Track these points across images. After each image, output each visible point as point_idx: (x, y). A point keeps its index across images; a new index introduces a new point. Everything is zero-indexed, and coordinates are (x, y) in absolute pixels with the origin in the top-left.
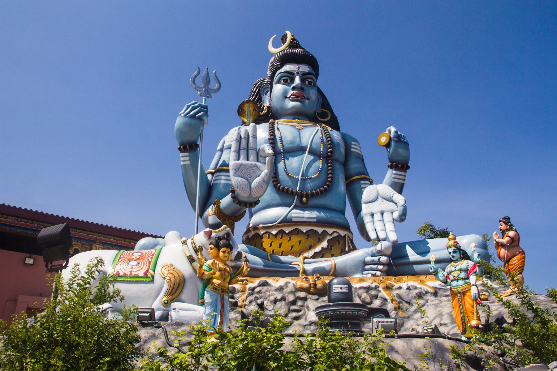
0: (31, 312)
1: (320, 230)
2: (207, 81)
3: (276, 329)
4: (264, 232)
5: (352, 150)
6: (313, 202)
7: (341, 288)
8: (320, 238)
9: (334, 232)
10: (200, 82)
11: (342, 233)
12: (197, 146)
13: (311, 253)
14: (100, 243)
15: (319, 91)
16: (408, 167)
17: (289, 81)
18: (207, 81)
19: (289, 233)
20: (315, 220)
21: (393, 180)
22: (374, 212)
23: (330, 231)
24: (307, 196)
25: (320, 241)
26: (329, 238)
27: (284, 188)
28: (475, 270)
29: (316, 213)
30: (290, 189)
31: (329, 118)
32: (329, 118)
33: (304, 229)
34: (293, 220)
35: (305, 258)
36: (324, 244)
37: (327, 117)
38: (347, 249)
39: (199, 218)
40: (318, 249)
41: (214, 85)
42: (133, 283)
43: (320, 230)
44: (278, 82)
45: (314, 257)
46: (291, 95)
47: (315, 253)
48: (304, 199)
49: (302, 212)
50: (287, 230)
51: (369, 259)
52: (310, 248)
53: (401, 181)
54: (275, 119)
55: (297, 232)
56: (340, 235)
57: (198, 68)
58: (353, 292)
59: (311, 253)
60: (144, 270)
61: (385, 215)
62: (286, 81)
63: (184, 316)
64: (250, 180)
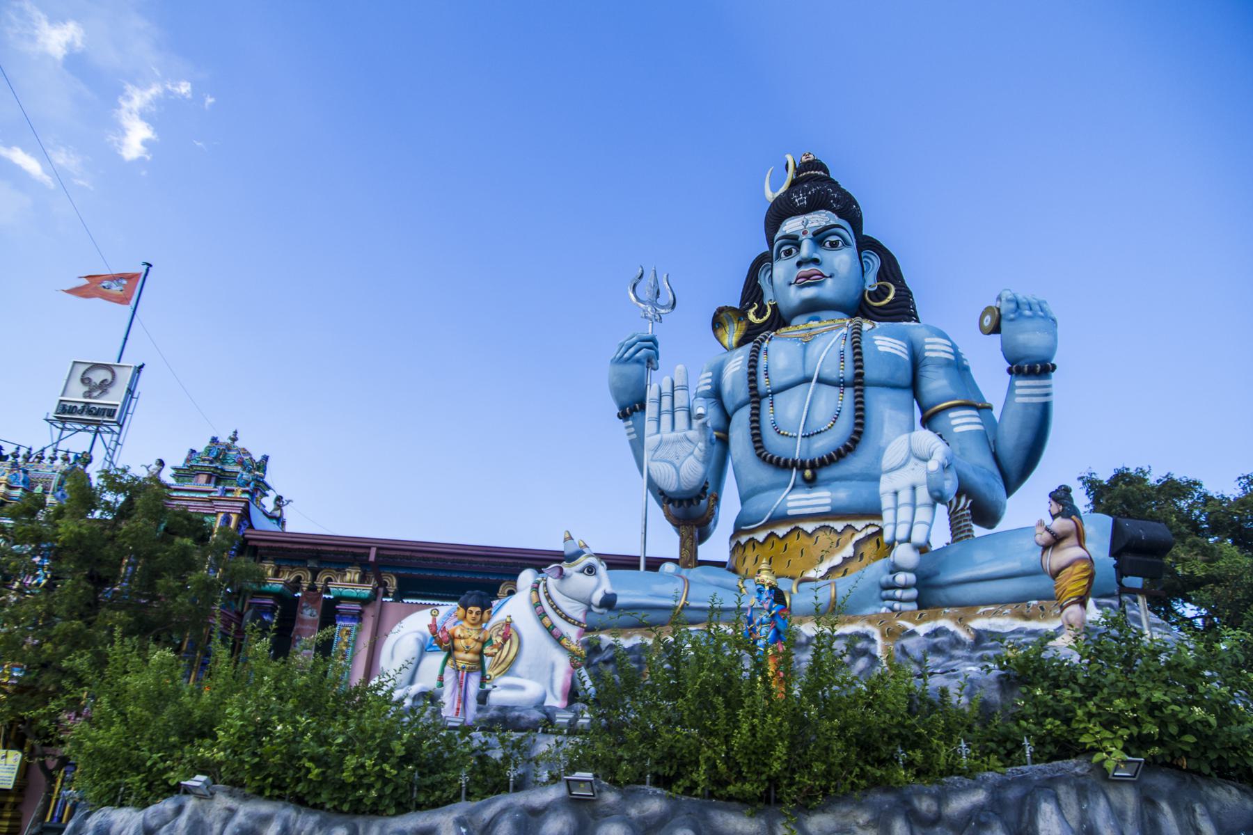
0: (328, 701)
4: (788, 529)
5: (927, 354)
6: (824, 474)
9: (867, 526)
19: (785, 536)
20: (827, 509)
22: (897, 487)
23: (859, 525)
24: (813, 466)
29: (827, 494)
31: (891, 297)
32: (891, 297)
33: (809, 527)
34: (790, 512)
36: (848, 551)
37: (887, 295)
40: (837, 560)
42: (1007, 572)
43: (839, 526)
50: (781, 531)
53: (1043, 400)
57: (236, 432)
59: (824, 568)
61: (900, 495)
64: (677, 463)
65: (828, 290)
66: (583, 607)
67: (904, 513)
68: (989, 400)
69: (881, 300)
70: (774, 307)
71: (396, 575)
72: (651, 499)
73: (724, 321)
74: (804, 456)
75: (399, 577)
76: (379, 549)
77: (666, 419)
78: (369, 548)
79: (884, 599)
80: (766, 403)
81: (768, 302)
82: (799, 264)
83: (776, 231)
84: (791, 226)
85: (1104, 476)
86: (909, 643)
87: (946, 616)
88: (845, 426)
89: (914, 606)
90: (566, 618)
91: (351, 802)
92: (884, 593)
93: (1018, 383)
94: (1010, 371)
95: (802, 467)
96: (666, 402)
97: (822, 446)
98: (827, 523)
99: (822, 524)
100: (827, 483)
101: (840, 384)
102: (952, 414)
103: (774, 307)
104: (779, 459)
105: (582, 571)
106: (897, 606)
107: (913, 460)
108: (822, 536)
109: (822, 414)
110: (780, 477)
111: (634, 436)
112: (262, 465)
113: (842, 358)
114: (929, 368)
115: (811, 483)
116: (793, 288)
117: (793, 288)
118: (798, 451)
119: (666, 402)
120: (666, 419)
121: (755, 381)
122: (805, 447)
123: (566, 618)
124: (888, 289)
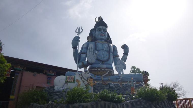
1: (106, 70)
2: (79, 30)
3: (55, 101)
6: (105, 63)
8: (106, 71)
10: (77, 31)
11: (112, 70)
13: (104, 75)
18: (79, 30)
20: (105, 67)
23: (109, 70)
24: (104, 61)
25: (106, 72)
26: (108, 71)
28: (132, 93)
29: (105, 65)
33: (103, 69)
34: (101, 67)
35: (103, 76)
36: (107, 73)
40: (106, 74)
41: (81, 31)
43: (106, 70)
47: (105, 75)
49: (102, 65)
50: (99, 69)
52: (104, 74)
54: (96, 40)
55: (101, 70)
56: (111, 71)
58: (12, 89)
59: (104, 75)
60: (73, 80)
65: (103, 37)
66: (87, 78)
72: (80, 61)
75: (114, 75)
77: (90, 52)
82: (101, 33)
83: (98, 27)
85: (145, 71)
86: (124, 85)
89: (120, 81)
90: (85, 80)
93: (125, 55)
95: (102, 61)
96: (90, 50)
97: (105, 59)
100: (105, 64)
101: (107, 51)
106: (119, 81)
112: (144, 71)
113: (108, 48)
115: (103, 64)
119: (90, 50)
120: (90, 52)
123: (85, 80)
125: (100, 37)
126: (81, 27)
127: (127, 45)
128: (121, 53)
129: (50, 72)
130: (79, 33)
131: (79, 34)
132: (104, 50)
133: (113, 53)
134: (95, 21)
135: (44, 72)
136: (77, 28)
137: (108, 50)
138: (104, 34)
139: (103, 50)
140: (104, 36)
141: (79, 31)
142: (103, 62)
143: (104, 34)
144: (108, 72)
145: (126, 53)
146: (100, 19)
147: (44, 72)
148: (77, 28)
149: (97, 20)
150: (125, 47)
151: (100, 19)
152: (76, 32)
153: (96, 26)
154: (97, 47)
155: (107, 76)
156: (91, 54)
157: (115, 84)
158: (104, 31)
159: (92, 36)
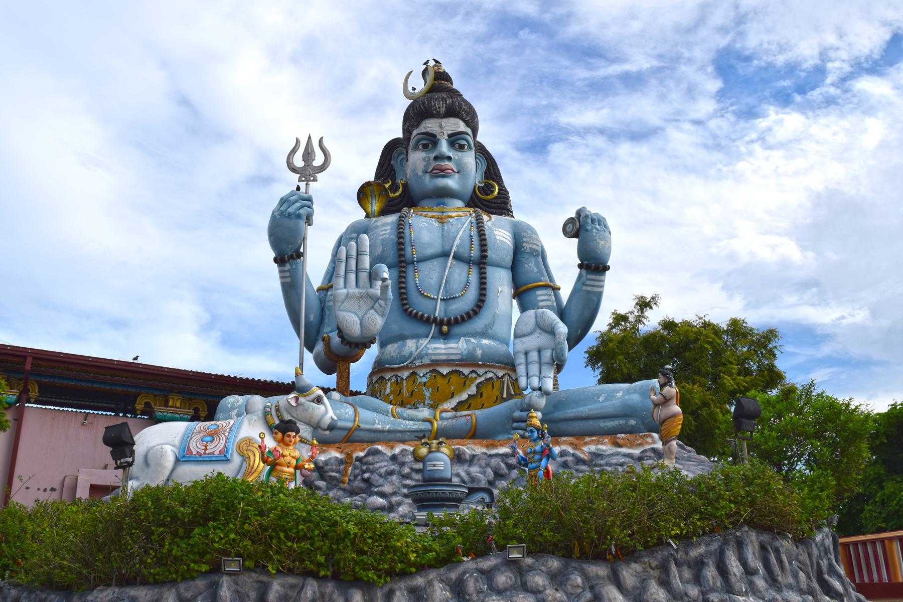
1: (466, 371)
2: (308, 155)
6: (457, 330)
7: (434, 466)
8: (465, 382)
10: (299, 162)
12: (300, 255)
14: (179, 392)
15: (481, 151)
16: (607, 268)
17: (430, 146)
18: (308, 155)
21: (602, 278)
23: (481, 371)
24: (449, 323)
25: (464, 386)
26: (479, 380)
27: (417, 313)
30: (426, 315)
36: (473, 390)
38: (505, 396)
39: (306, 351)
40: (464, 396)
41: (319, 160)
43: (466, 371)
44: (416, 148)
45: (455, 409)
46: (433, 169)
48: (445, 328)
51: (517, 414)
59: (454, 402)
62: (425, 147)
63: (568, 124)
67: (534, 369)
68: (558, 283)
69: (487, 195)
70: (406, 186)
71: (206, 402)
73: (369, 192)
74: (443, 315)
76: (34, 358)
78: (25, 357)
79: (515, 429)
80: (410, 269)
81: (400, 182)
82: (436, 158)
83: (417, 126)
84: (430, 125)
87: (565, 443)
88: (472, 294)
91: (345, 579)
92: (515, 425)
94: (580, 266)
95: (440, 323)
98: (458, 368)
99: (454, 368)
100: (458, 337)
101: (468, 261)
102: (539, 292)
103: (406, 186)
104: (422, 315)
105: (313, 401)
107: (538, 331)
108: (454, 378)
109: (457, 284)
110: (422, 329)
111: (289, 280)
114: (526, 256)
115: (445, 336)
116: (428, 176)
117: (428, 176)
118: (439, 311)
119: (353, 262)
120: (352, 276)
121: (481, 273)
122: (443, 309)
124: (493, 187)
125: (430, 183)
126: (322, 138)
127: (592, 209)
128: (562, 261)
129: (170, 403)
130: (308, 173)
131: (308, 181)
132: (449, 256)
133: (514, 268)
134: (407, 94)
135: (139, 406)
136: (298, 141)
137: (475, 253)
138: (450, 165)
139: (445, 255)
140: (457, 175)
141: (308, 164)
142: (445, 328)
143: (450, 165)
144: (478, 386)
145: (593, 265)
146: (439, 81)
147: (139, 406)
148: (298, 141)
149: (419, 85)
150: (580, 227)
151: (439, 81)
152: (294, 169)
153: (415, 115)
154: (407, 241)
155: (469, 408)
156: (357, 285)
157: (497, 455)
158: (457, 146)
159: (392, 189)
